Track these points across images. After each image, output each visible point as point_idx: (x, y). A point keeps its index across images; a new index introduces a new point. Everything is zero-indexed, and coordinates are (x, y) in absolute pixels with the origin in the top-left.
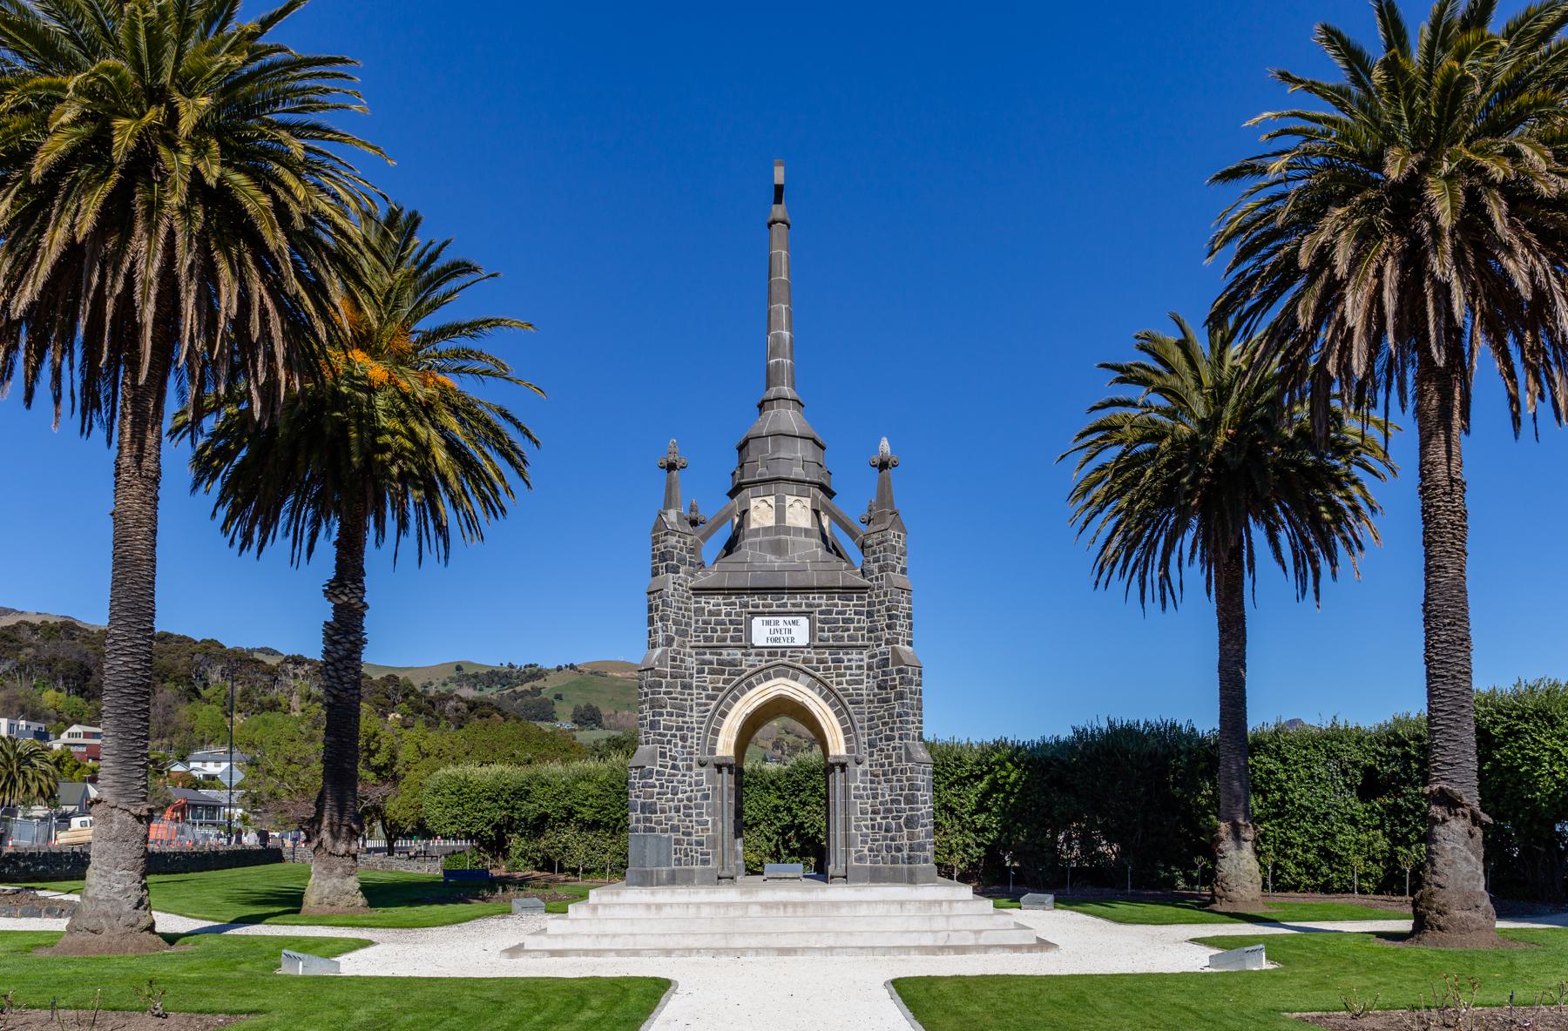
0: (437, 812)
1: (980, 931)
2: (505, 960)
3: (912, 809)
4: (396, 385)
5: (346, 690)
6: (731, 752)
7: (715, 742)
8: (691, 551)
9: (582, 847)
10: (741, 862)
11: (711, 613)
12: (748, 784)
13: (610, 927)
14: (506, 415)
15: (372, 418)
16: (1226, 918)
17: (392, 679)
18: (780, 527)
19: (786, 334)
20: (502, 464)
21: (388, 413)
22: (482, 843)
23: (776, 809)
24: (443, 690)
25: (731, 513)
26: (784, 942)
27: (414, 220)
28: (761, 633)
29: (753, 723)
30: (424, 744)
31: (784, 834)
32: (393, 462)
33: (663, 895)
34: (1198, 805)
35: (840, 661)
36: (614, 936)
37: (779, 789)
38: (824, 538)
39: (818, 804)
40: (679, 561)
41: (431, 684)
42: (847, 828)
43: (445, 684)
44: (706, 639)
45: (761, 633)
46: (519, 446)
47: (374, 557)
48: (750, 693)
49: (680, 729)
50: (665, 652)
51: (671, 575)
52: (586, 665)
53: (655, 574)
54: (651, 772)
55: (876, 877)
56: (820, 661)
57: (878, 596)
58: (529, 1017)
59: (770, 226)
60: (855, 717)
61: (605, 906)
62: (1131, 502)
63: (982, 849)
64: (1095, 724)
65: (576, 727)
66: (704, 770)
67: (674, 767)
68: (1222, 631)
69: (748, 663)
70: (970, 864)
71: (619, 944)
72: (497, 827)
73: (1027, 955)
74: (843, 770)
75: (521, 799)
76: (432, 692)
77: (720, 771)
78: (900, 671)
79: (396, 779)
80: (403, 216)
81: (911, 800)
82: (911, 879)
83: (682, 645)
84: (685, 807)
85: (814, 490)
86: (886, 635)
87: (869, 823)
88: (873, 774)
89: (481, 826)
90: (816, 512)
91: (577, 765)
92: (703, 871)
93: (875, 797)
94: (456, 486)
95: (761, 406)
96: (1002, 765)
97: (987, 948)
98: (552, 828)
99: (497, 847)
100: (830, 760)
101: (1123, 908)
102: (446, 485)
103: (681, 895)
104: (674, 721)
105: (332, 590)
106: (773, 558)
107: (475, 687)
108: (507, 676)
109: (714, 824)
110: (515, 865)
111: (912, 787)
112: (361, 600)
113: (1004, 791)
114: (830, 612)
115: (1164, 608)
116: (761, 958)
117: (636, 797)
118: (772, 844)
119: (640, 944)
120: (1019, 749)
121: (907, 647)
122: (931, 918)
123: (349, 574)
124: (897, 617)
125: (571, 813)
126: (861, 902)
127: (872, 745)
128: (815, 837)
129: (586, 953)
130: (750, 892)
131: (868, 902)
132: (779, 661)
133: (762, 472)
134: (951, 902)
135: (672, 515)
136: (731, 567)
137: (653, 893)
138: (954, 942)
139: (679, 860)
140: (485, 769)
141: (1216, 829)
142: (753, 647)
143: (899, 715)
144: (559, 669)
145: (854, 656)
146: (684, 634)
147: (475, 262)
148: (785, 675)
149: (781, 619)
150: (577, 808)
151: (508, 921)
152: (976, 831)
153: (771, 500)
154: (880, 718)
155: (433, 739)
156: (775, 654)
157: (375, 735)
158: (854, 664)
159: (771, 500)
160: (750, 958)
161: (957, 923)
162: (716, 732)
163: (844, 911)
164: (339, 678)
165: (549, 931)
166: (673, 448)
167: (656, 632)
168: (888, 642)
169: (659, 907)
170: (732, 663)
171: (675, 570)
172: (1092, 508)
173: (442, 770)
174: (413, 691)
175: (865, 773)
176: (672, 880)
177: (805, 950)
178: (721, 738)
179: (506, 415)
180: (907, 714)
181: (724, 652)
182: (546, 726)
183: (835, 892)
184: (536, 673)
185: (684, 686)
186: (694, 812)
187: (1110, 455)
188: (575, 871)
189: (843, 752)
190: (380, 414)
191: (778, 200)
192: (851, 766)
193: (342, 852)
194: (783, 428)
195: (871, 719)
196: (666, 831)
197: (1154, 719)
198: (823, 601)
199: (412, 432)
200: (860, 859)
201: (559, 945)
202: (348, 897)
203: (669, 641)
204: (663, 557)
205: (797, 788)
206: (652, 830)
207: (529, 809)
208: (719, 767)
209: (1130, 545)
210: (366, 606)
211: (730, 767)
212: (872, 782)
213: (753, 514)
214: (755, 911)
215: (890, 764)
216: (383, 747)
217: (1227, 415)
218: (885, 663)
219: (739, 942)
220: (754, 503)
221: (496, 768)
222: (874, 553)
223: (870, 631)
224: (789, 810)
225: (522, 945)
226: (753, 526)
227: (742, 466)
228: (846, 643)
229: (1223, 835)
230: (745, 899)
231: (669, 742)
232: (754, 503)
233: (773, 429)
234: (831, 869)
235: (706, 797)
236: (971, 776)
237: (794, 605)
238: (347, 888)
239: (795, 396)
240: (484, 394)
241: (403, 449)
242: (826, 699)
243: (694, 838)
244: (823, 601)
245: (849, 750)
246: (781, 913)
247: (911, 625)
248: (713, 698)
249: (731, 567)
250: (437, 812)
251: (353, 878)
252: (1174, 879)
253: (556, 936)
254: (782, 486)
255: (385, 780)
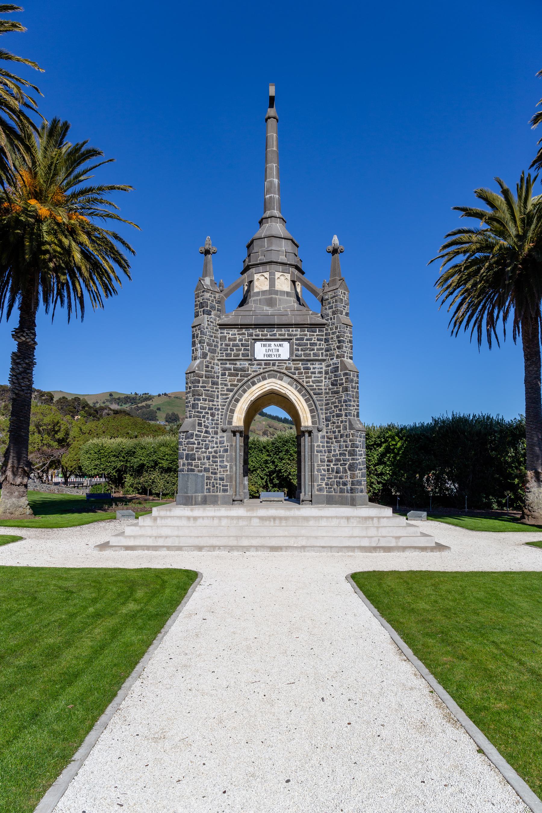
0: (87, 463)
1: (399, 537)
2: (96, 553)
3: (353, 459)
4: (54, 219)
5: (23, 390)
6: (241, 424)
7: (231, 418)
8: (219, 302)
9: (162, 482)
10: (246, 491)
11: (230, 340)
12: (251, 448)
13: (165, 531)
14: (116, 237)
15: (40, 236)
16: (536, 528)
17: (77, 399)
18: (272, 290)
19: (276, 181)
20: (115, 266)
21: (49, 233)
22: (111, 480)
23: (266, 462)
24: (103, 405)
25: (241, 284)
26: (274, 542)
27: (66, 127)
28: (260, 351)
29: (255, 409)
30: (83, 428)
31: (270, 475)
32: (50, 260)
33: (198, 511)
34: (506, 462)
35: (308, 369)
36: (166, 537)
37: (268, 451)
38: (298, 299)
39: (289, 459)
40: (211, 307)
41: (97, 402)
42: (312, 471)
43: (104, 403)
44: (227, 355)
45: (260, 351)
46: (125, 257)
47: (41, 316)
48: (254, 388)
49: (211, 409)
50: (202, 362)
51: (206, 316)
52: (172, 394)
53: (197, 316)
54: (192, 435)
55: (330, 501)
56: (297, 369)
57: (331, 329)
58: (85, 608)
59: (266, 120)
60: (317, 403)
61: (162, 518)
62: (475, 285)
63: (381, 485)
64: (445, 415)
65: (167, 423)
66: (225, 434)
67: (206, 432)
68: (527, 360)
69: (253, 369)
70: (374, 493)
71: (169, 542)
72: (119, 471)
73: (430, 554)
74: (310, 435)
75: (131, 456)
76: (98, 406)
77: (235, 435)
78: (345, 374)
79: (68, 445)
80: (60, 125)
81: (352, 453)
82: (353, 503)
83: (213, 358)
84: (213, 457)
85: (292, 269)
86: (337, 352)
87: (326, 467)
88: (328, 438)
89: (110, 470)
90: (294, 282)
91: (161, 438)
92: (224, 497)
93: (329, 452)
94: (86, 274)
95: (261, 222)
96: (393, 438)
97: (404, 549)
98: (147, 471)
99: (118, 481)
100: (302, 429)
101: (468, 520)
102: (81, 274)
103: (210, 511)
104: (207, 404)
105: (17, 334)
106: (268, 308)
107: (118, 404)
108: (134, 399)
109: (231, 467)
110: (127, 491)
111: (353, 445)
112: (33, 340)
113: (394, 453)
114: (302, 339)
115: (490, 347)
116: (259, 553)
117: (183, 451)
118: (264, 481)
119: (183, 542)
120: (402, 429)
121: (349, 360)
122: (367, 528)
123: (27, 326)
124: (344, 341)
125: (156, 463)
126: (322, 517)
127: (327, 420)
128: (287, 477)
129: (148, 548)
130: (252, 510)
131: (327, 518)
132: (271, 368)
133: (261, 258)
134: (379, 518)
135: (207, 281)
136: (242, 313)
137: (192, 510)
138: (382, 544)
139: (209, 489)
140: (113, 440)
141: (525, 475)
142: (256, 360)
143: (345, 401)
144: (159, 395)
145: (317, 366)
146: (213, 351)
147: (99, 149)
148: (275, 377)
149: (272, 343)
150: (160, 461)
151: (112, 524)
152: (378, 475)
153: (267, 275)
154: (333, 403)
155: (91, 425)
156: (269, 364)
157: (58, 422)
158: (317, 370)
159: (267, 275)
160: (252, 553)
161: (383, 532)
162: (232, 411)
163: (311, 523)
164: (19, 384)
165: (126, 534)
166: (208, 243)
167: (197, 350)
168: (338, 357)
169: (195, 518)
170: (243, 370)
171: (209, 313)
172: (451, 289)
173: (91, 441)
174: (87, 405)
175: (323, 437)
176: (205, 502)
177: (287, 548)
178: (236, 415)
179: (116, 237)
180: (350, 401)
181: (238, 363)
182: (152, 422)
183: (305, 511)
184: (148, 398)
185: (214, 383)
186: (218, 460)
187: (460, 259)
188: (158, 495)
189: (309, 423)
190: (45, 234)
191: (271, 106)
192: (315, 432)
193: (18, 483)
194: (274, 233)
195: (327, 404)
196: (201, 471)
197: (478, 413)
198: (298, 332)
199: (60, 241)
200: (320, 490)
201: (131, 543)
202: (21, 509)
203: (204, 356)
204: (202, 305)
205: (278, 451)
206: (193, 470)
207: (135, 461)
208: (234, 433)
209: (472, 307)
210: (35, 343)
211: (241, 432)
212: (327, 442)
213: (256, 283)
214: (255, 522)
215: (339, 431)
216: (62, 429)
217: (530, 234)
218: (336, 369)
219: (245, 542)
220: (256, 276)
221: (119, 440)
222: (329, 303)
223: (327, 350)
224: (273, 462)
225: (108, 542)
226: (256, 290)
227: (249, 256)
228: (312, 357)
229: (529, 478)
230: (249, 514)
231: (204, 417)
232: (256, 276)
233: (268, 234)
234: (302, 496)
235: (226, 451)
236: (375, 444)
237: (280, 335)
238: (21, 504)
239: (281, 216)
240: (105, 227)
241: (55, 251)
242: (300, 391)
243: (218, 476)
244: (298, 333)
245: (313, 423)
246: (272, 523)
247: (352, 346)
248: (231, 391)
249: (242, 313)
250: (87, 463)
251: (25, 498)
252: (492, 503)
253: (130, 537)
254: (273, 266)
255: (63, 446)
